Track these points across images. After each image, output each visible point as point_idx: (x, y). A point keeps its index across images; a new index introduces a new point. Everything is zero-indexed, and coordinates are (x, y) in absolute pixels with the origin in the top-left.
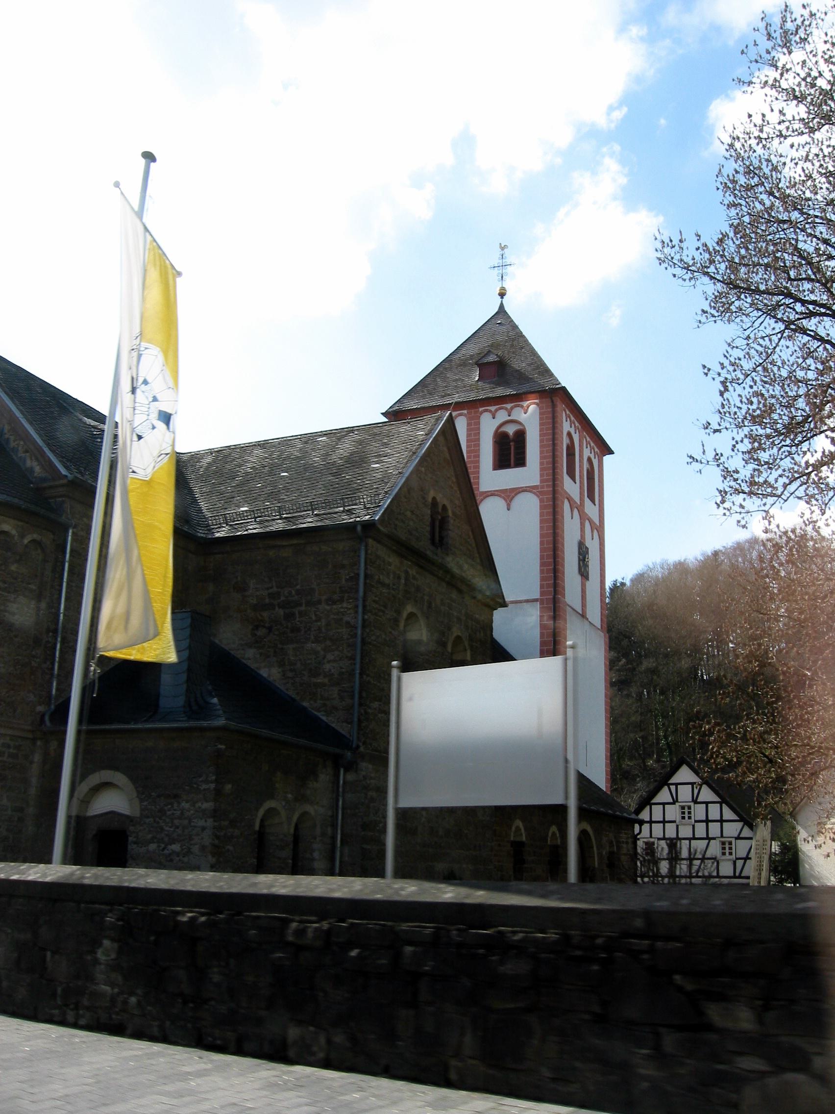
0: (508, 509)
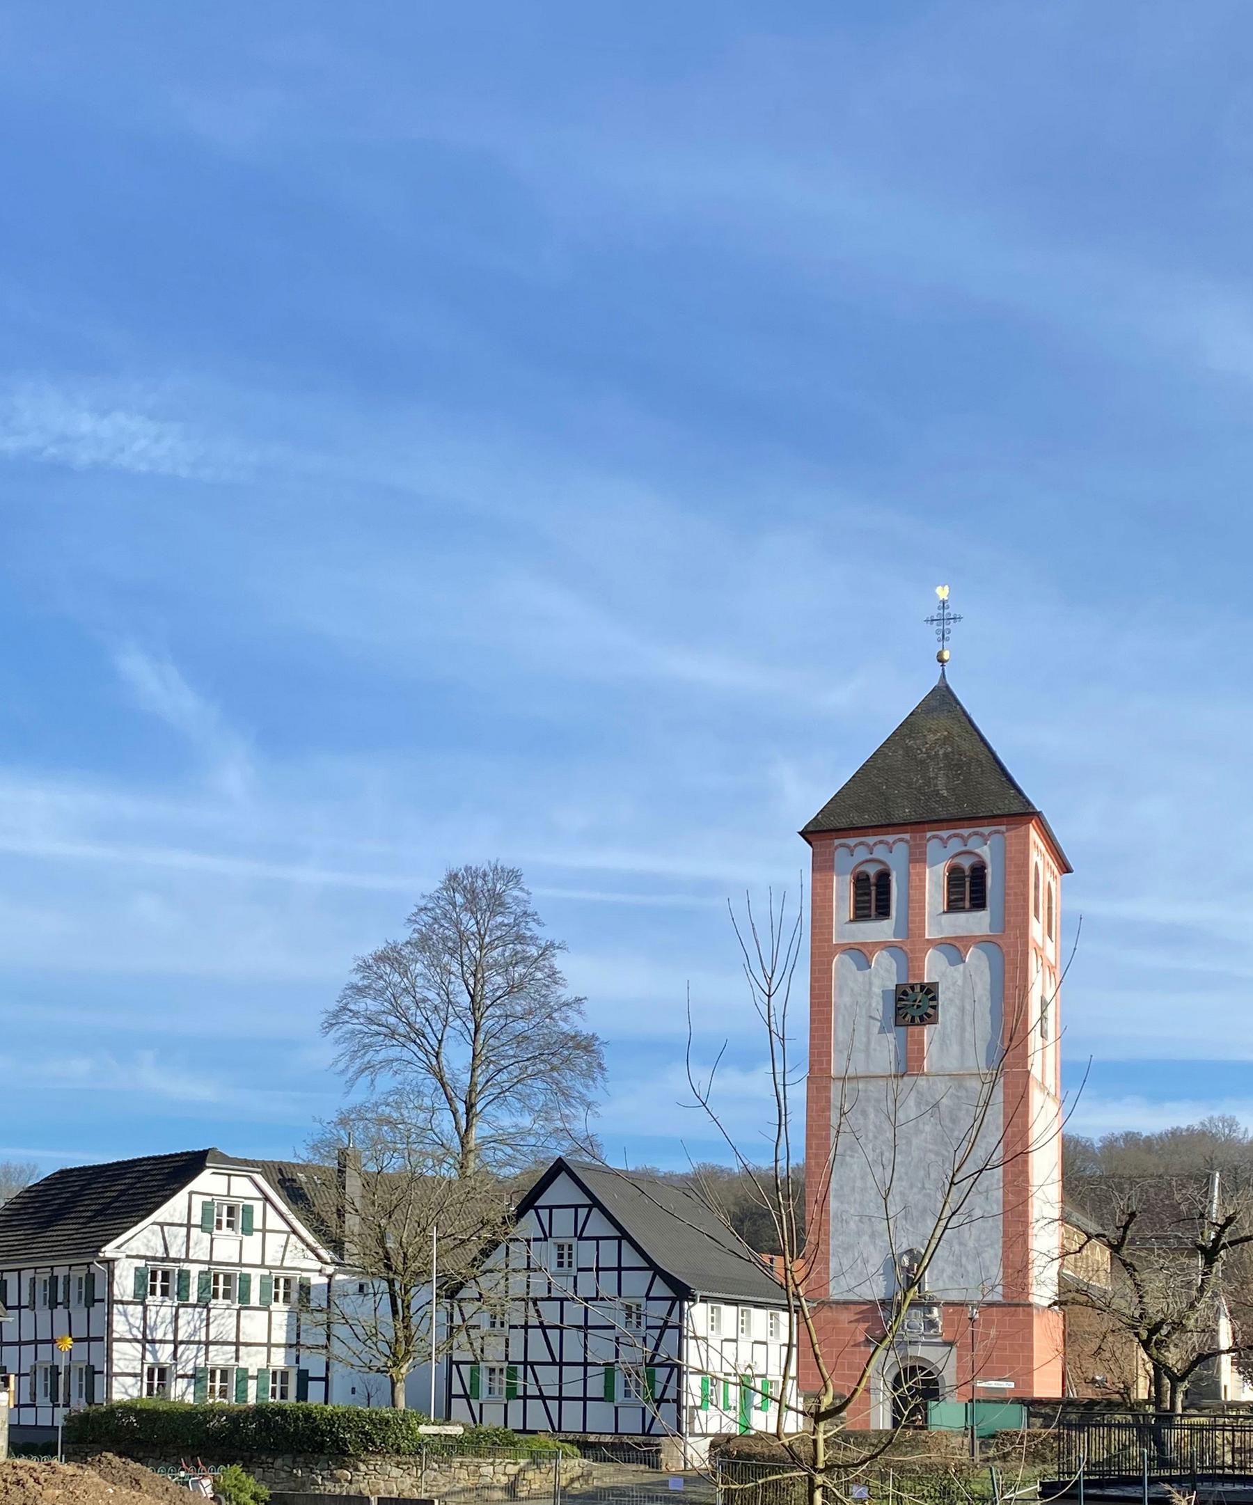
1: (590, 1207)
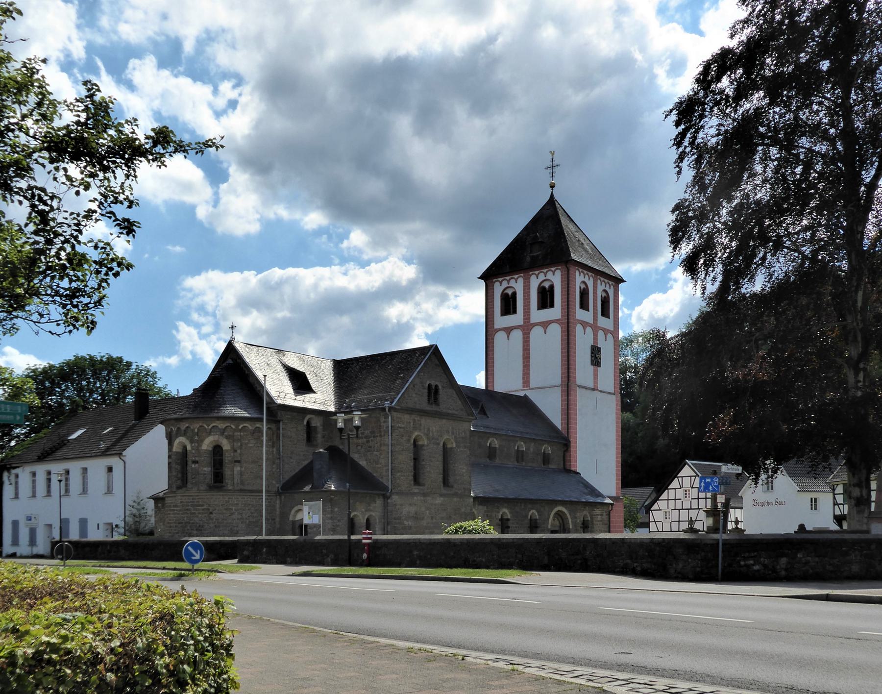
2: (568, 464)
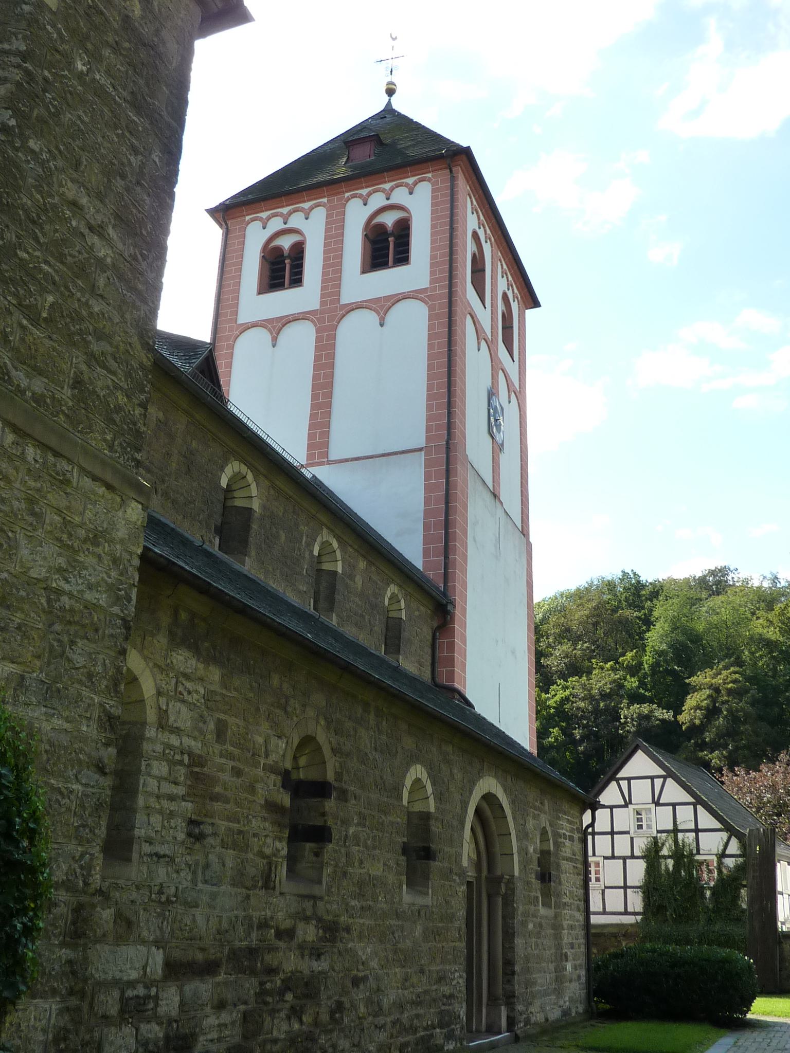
0: (382, 325)
1: (665, 778)
2: (442, 670)
